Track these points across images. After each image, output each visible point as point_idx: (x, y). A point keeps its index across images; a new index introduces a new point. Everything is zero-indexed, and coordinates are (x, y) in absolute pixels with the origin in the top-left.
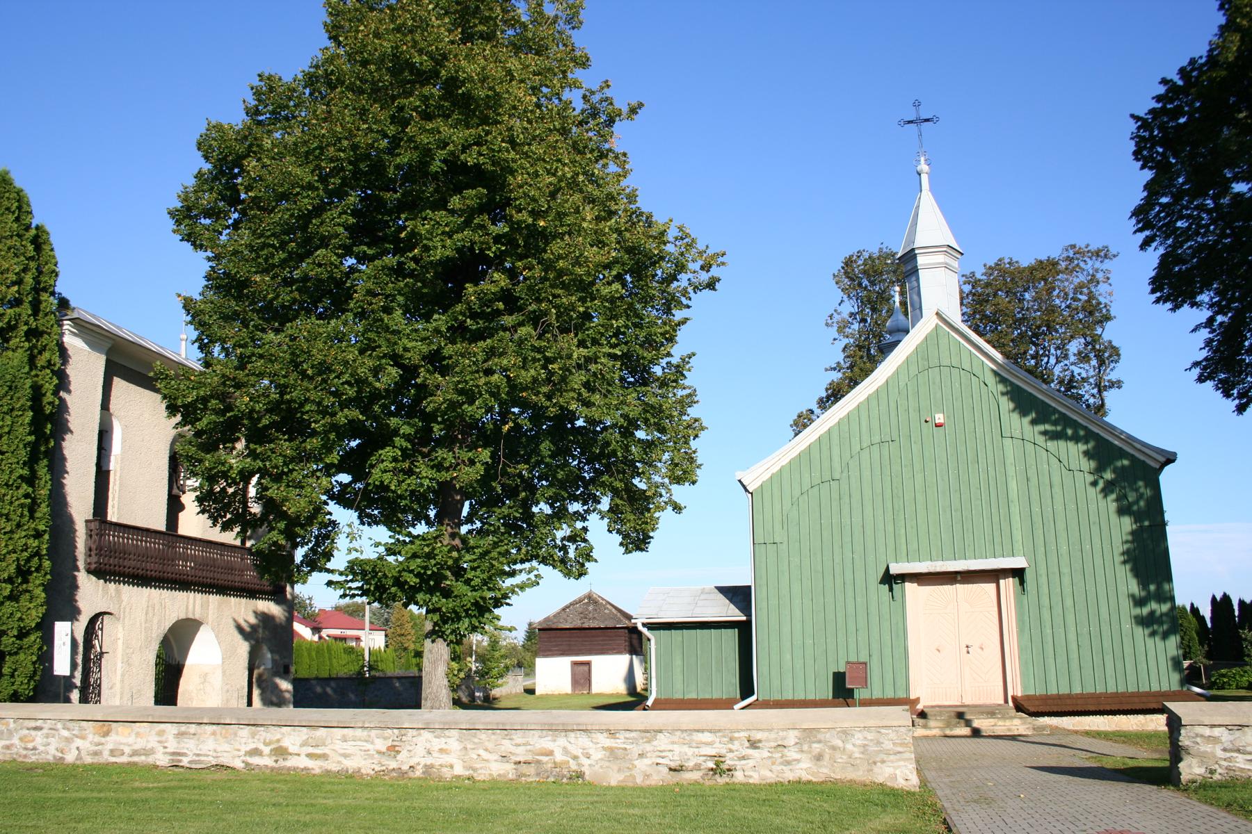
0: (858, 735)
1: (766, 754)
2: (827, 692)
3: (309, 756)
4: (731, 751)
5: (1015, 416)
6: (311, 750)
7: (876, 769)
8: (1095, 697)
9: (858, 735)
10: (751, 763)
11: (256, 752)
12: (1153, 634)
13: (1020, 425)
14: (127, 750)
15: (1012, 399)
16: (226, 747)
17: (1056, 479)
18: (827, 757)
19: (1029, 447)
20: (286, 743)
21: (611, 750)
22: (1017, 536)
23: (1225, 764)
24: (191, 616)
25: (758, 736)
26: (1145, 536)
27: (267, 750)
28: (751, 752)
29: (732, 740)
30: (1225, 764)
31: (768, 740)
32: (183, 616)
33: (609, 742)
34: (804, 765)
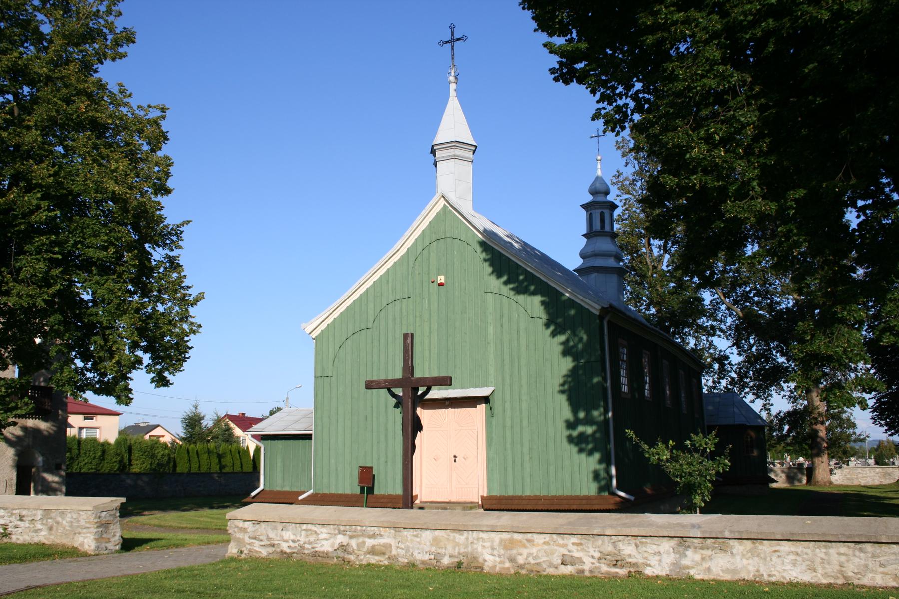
0: (69, 515)
1: (28, 525)
2: (350, 485)
4: (11, 522)
5: (493, 278)
7: (76, 538)
8: (537, 498)
9: (69, 515)
10: (20, 530)
12: (581, 451)
13: (496, 283)
15: (491, 265)
17: (522, 326)
18: (55, 528)
19: (505, 299)
22: (492, 371)
23: (248, 547)
25: (24, 513)
26: (581, 372)
28: (19, 523)
29: (12, 514)
30: (248, 547)
31: (28, 516)
34: (43, 533)
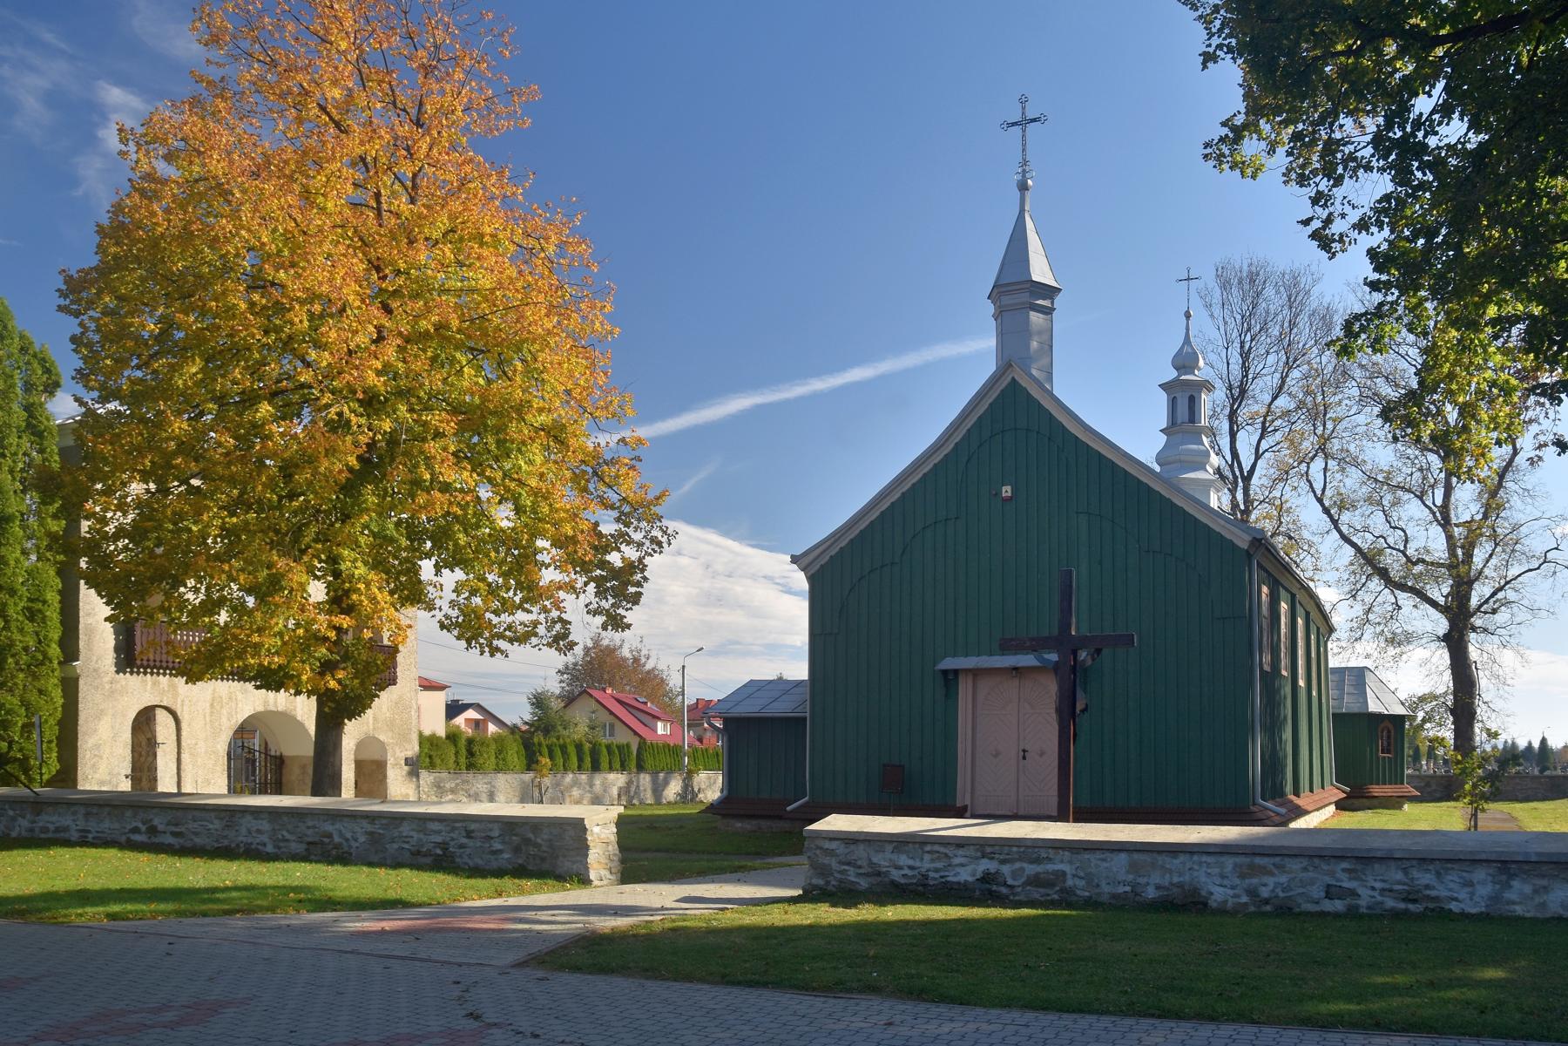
3: (174, 834)
6: (174, 829)
10: (468, 851)
11: (136, 830)
14: (52, 827)
16: (116, 826)
20: (156, 822)
21: (371, 833)
24: (272, 708)
27: (143, 828)
32: (260, 709)
33: (370, 828)
34: (506, 856)
